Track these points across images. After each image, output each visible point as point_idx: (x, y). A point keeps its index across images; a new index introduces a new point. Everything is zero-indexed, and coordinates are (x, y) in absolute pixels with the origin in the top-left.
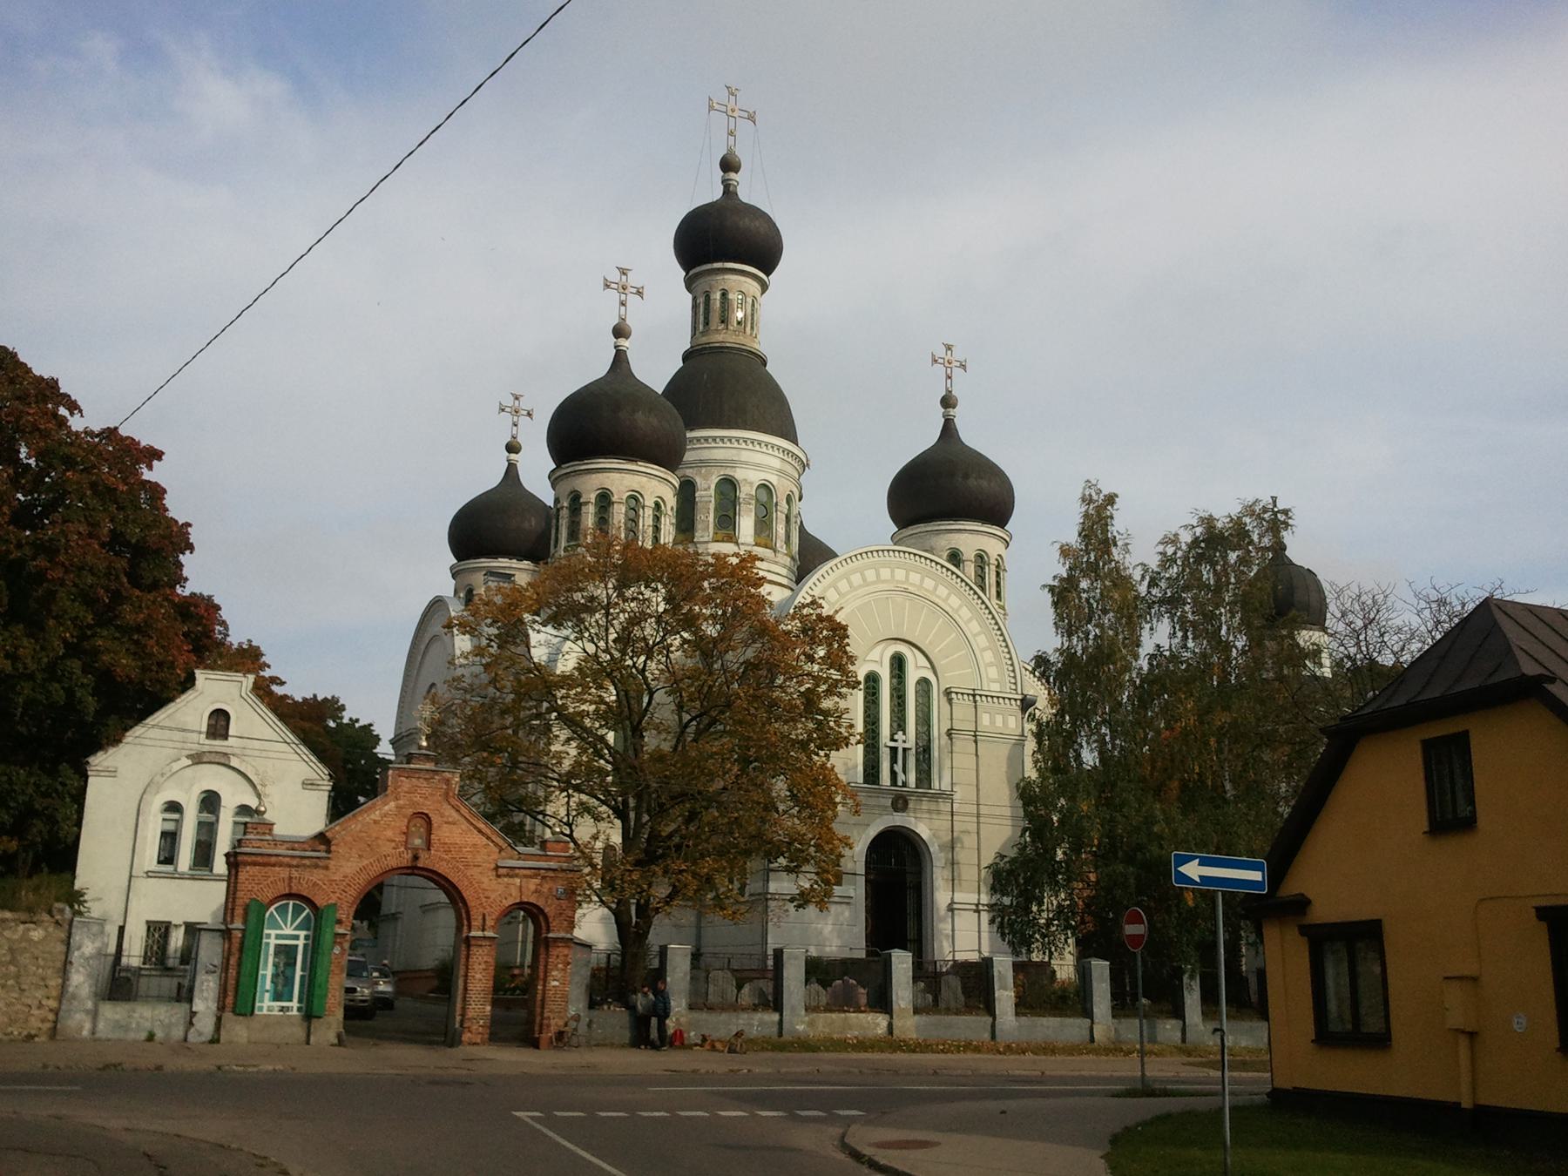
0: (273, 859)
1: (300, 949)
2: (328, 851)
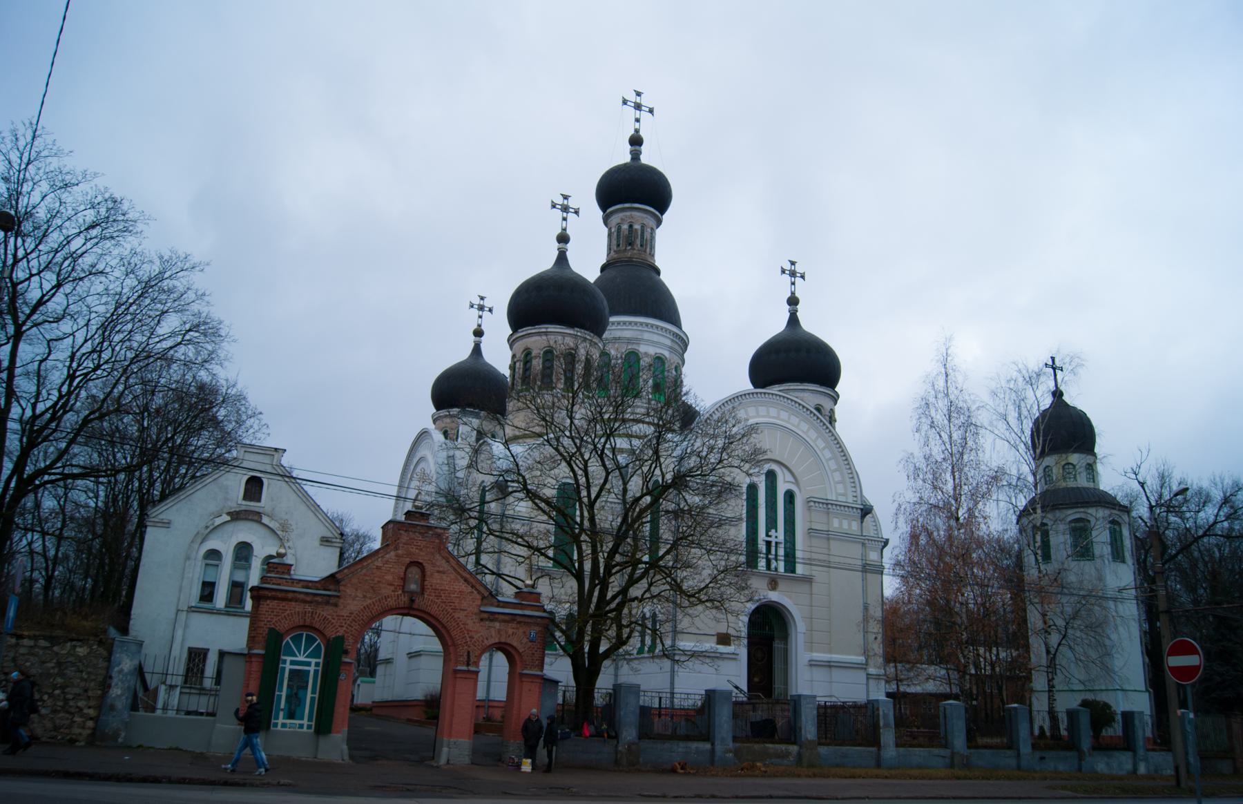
0: (290, 595)
1: (312, 673)
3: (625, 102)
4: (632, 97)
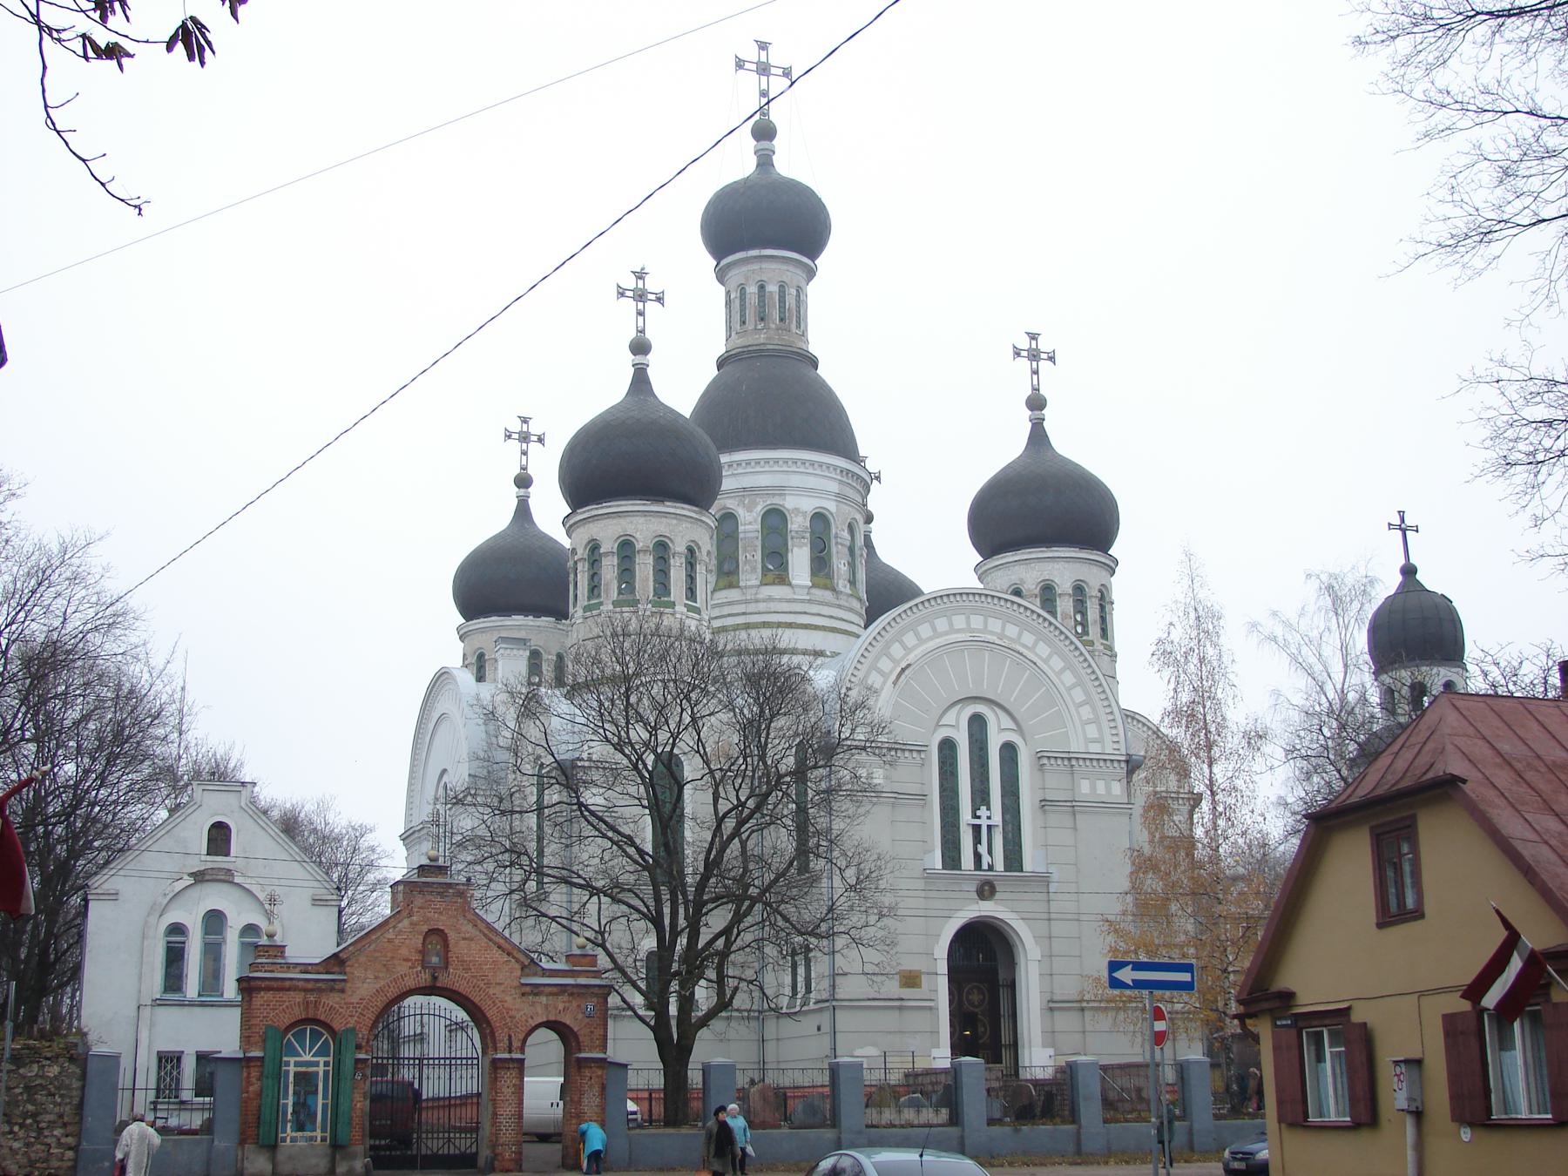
0: (287, 984)
3: (740, 64)
4: (751, 53)
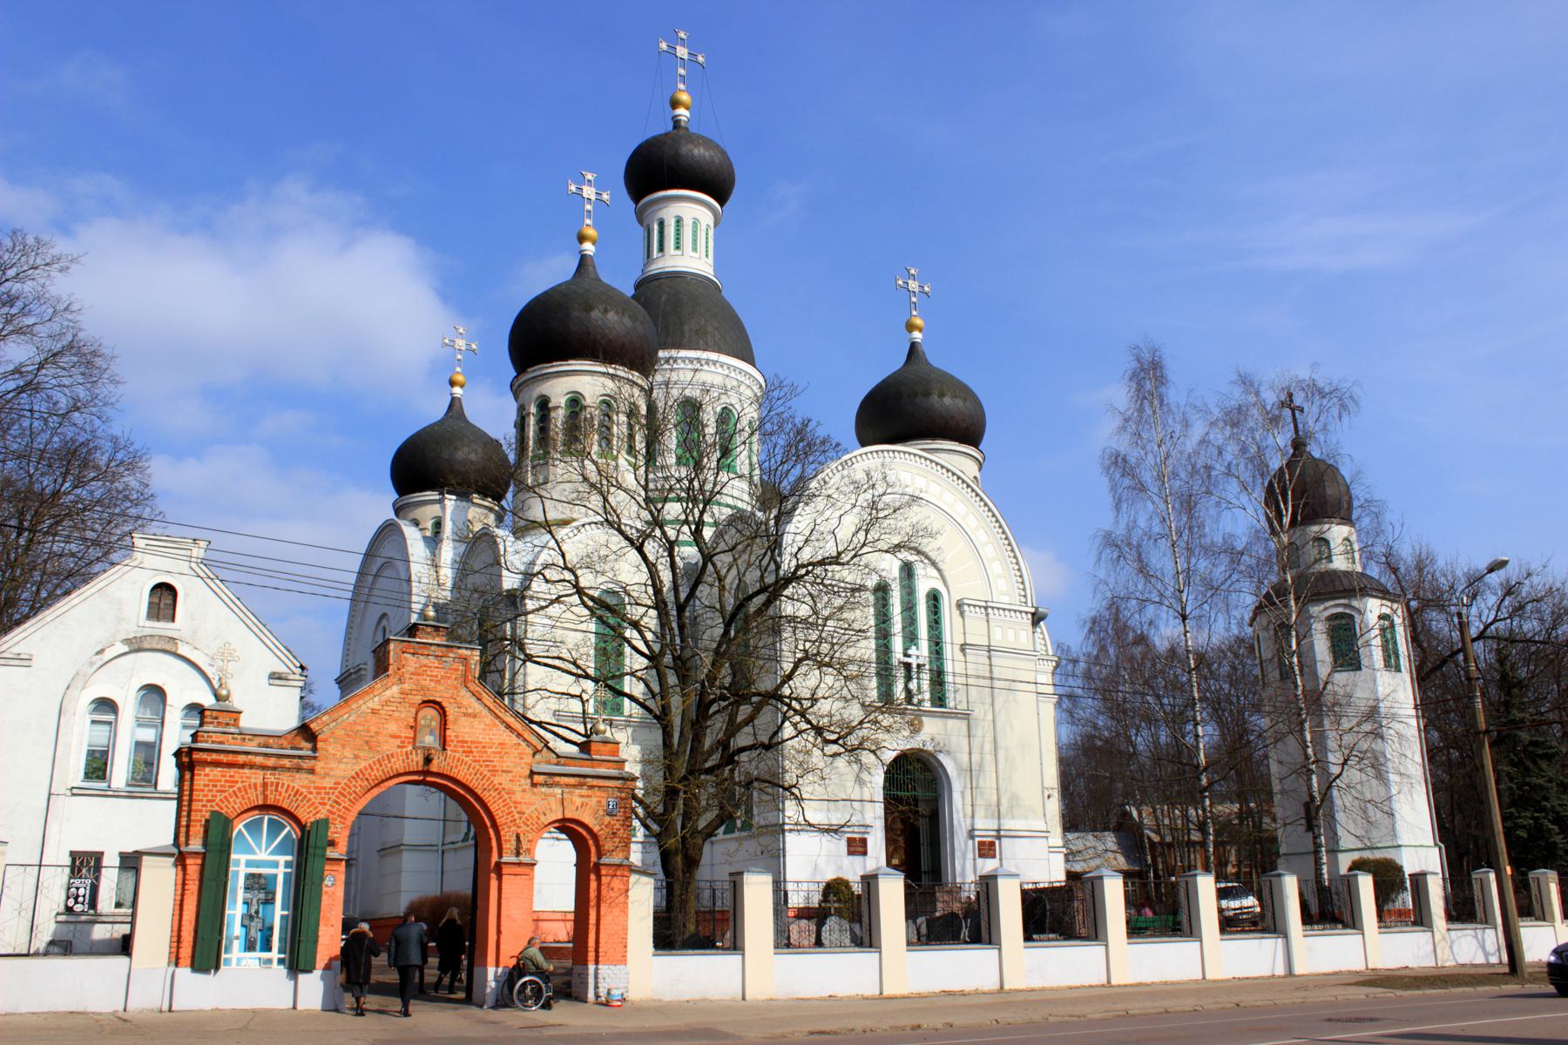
0: (241, 759)
1: (280, 879)
2: (315, 749)
